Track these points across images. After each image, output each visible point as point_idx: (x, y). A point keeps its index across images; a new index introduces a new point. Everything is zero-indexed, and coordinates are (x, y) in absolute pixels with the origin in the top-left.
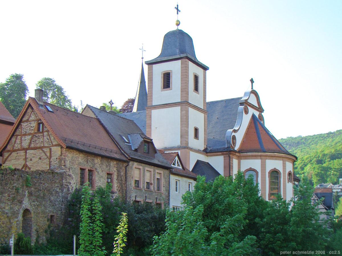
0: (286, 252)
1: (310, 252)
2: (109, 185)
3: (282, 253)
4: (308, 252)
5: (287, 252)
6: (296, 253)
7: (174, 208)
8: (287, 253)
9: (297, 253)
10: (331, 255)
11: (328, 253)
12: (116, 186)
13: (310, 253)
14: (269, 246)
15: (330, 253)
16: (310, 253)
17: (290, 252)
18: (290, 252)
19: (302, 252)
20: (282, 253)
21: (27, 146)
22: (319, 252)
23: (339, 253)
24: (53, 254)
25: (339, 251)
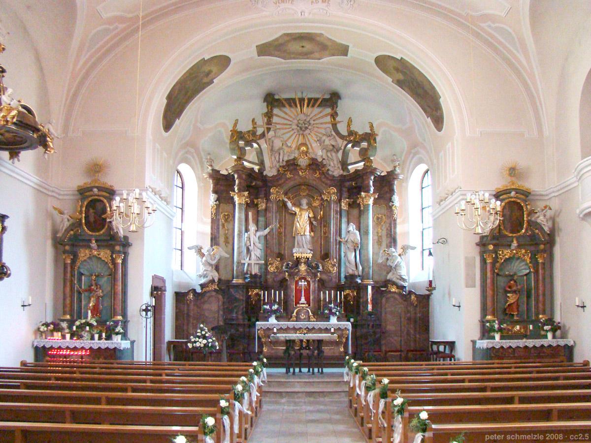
0: (495, 435)
1: (536, 436)
2: (326, 115)
3: (487, 437)
4: (533, 437)
5: (539, 435)
6: (576, 437)
7: (474, 204)
8: (498, 437)
9: (515, 437)
10: (574, 440)
11: (569, 437)
12: (344, 226)
13: (537, 437)
14: (108, 323)
15: (572, 437)
16: (537, 437)
17: (503, 436)
18: (503, 436)
19: (525, 437)
20: (487, 437)
21: (528, 242)
22: (552, 436)
23: (587, 438)
24: (82, 441)
25: (586, 435)
